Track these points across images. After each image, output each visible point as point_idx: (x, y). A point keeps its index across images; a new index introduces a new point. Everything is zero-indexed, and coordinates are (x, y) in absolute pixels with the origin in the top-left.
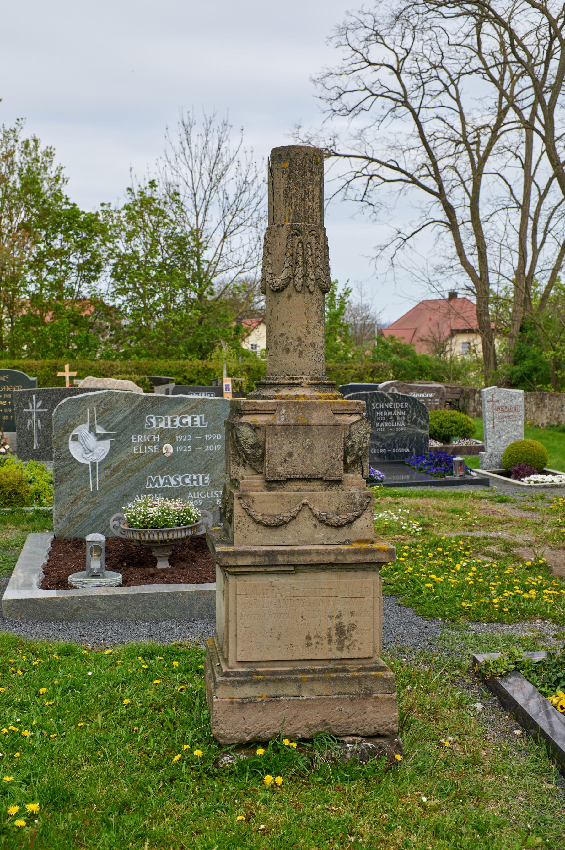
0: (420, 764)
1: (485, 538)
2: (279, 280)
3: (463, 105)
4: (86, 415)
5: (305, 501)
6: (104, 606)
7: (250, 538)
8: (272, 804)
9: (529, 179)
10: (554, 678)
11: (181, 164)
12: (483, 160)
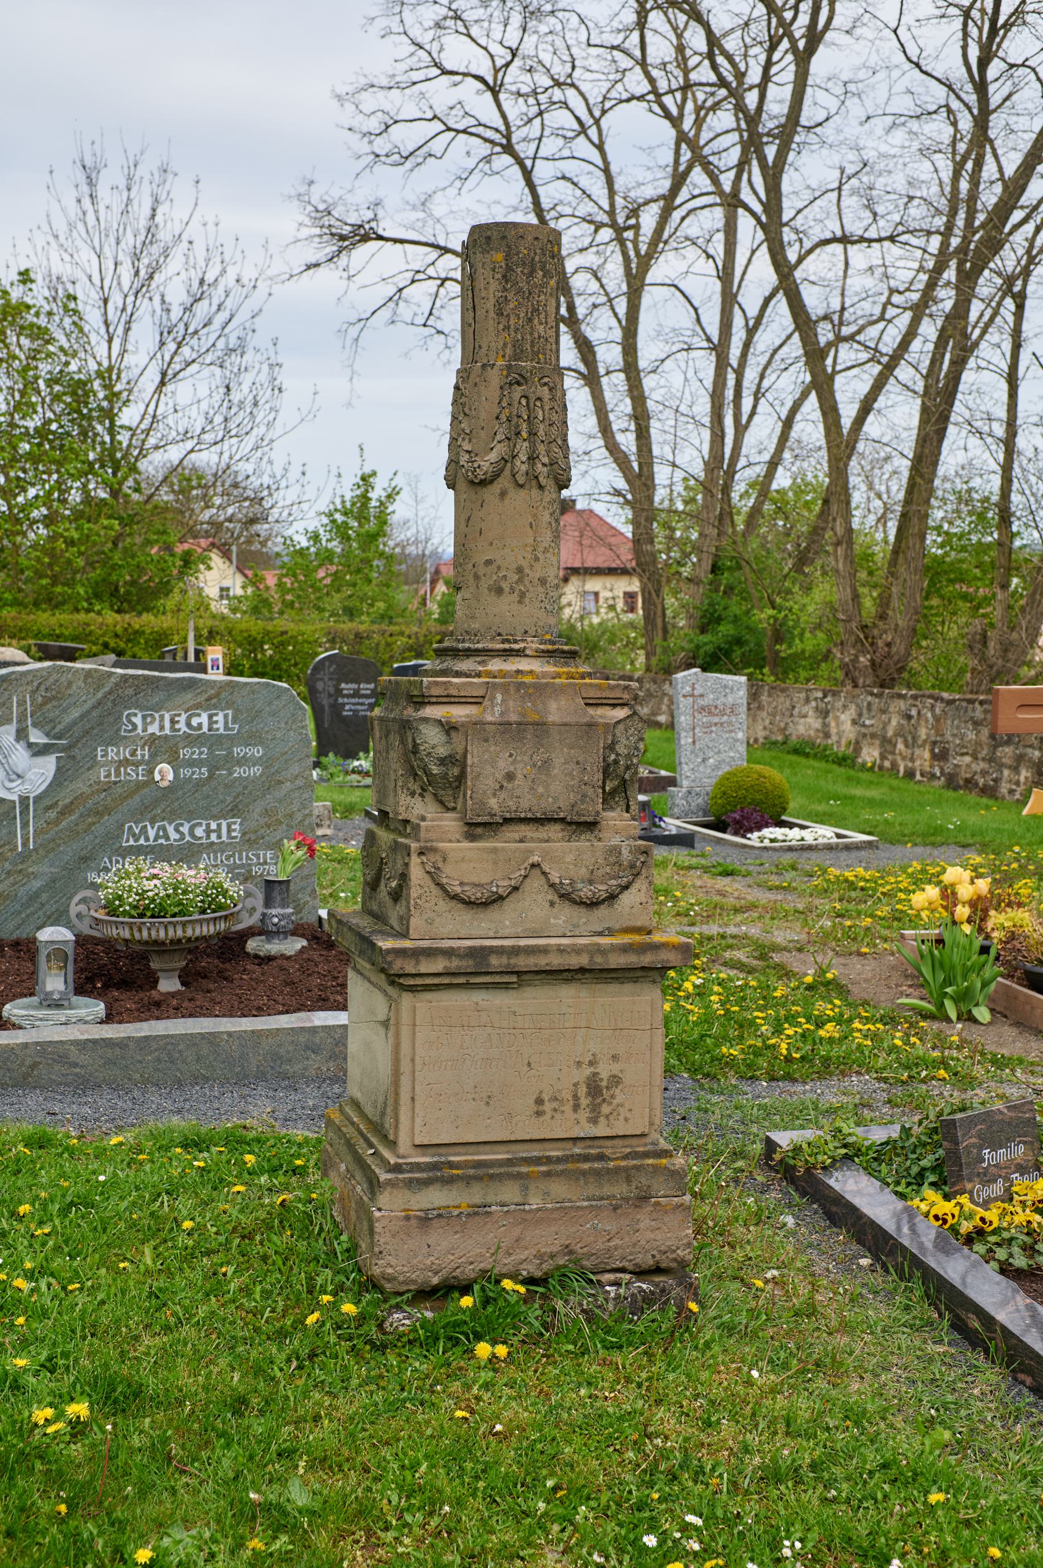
0: (726, 1318)
1: (723, 937)
2: (487, 462)
3: (610, 158)
4: (11, 709)
5: (536, 859)
6: (84, 1059)
7: (436, 924)
8: (497, 1392)
9: (729, 299)
10: (915, 1170)
11: (79, 243)
12: (646, 261)
